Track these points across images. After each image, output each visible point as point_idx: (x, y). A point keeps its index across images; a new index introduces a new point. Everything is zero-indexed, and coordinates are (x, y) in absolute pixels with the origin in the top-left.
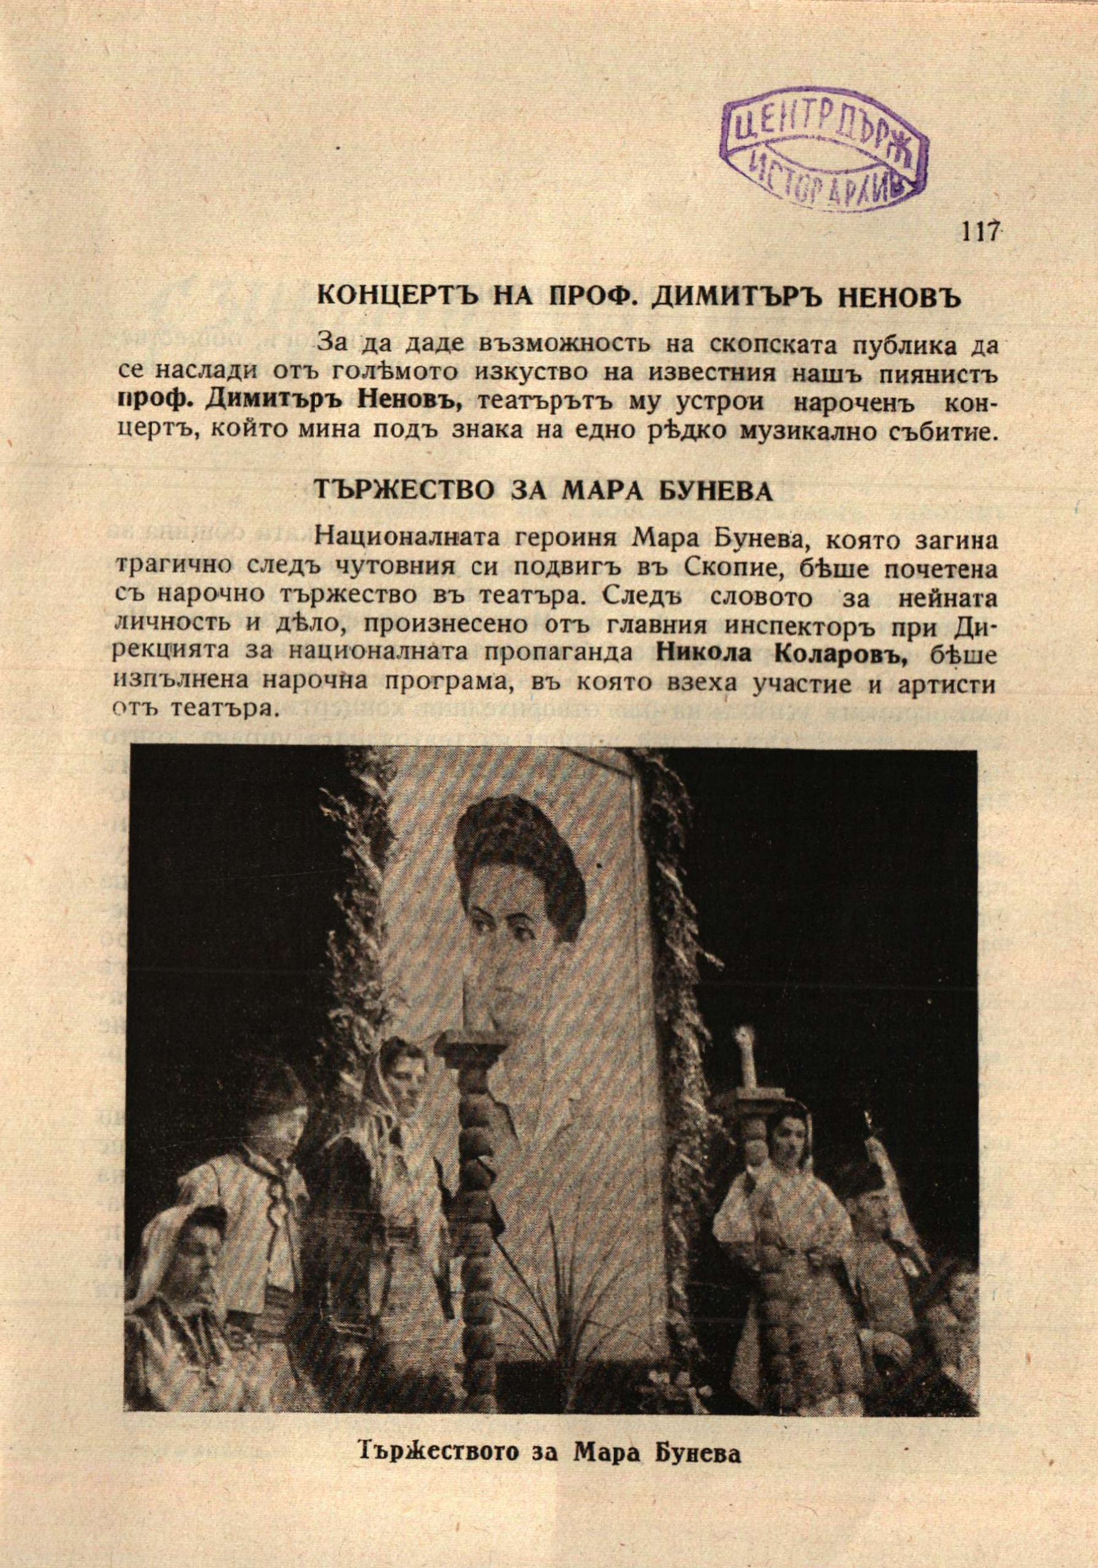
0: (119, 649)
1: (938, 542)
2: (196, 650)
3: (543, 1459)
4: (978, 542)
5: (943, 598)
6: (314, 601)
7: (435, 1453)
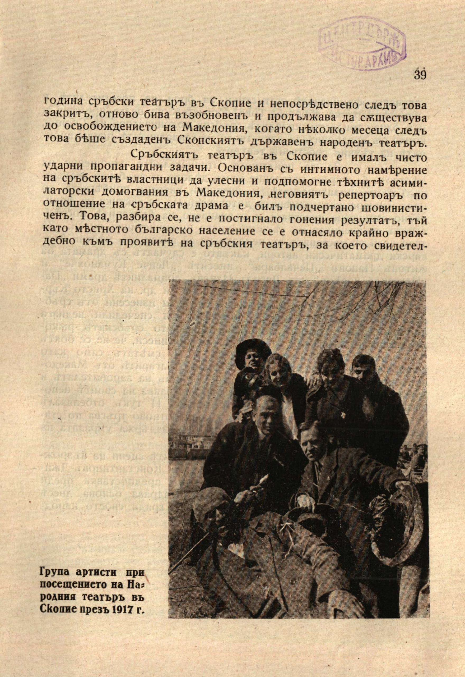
0: (119, 217)
1: (122, 166)
2: (312, 195)
3: (50, 116)
4: (417, 106)
5: (375, 233)
6: (411, 146)
7: (91, 598)
